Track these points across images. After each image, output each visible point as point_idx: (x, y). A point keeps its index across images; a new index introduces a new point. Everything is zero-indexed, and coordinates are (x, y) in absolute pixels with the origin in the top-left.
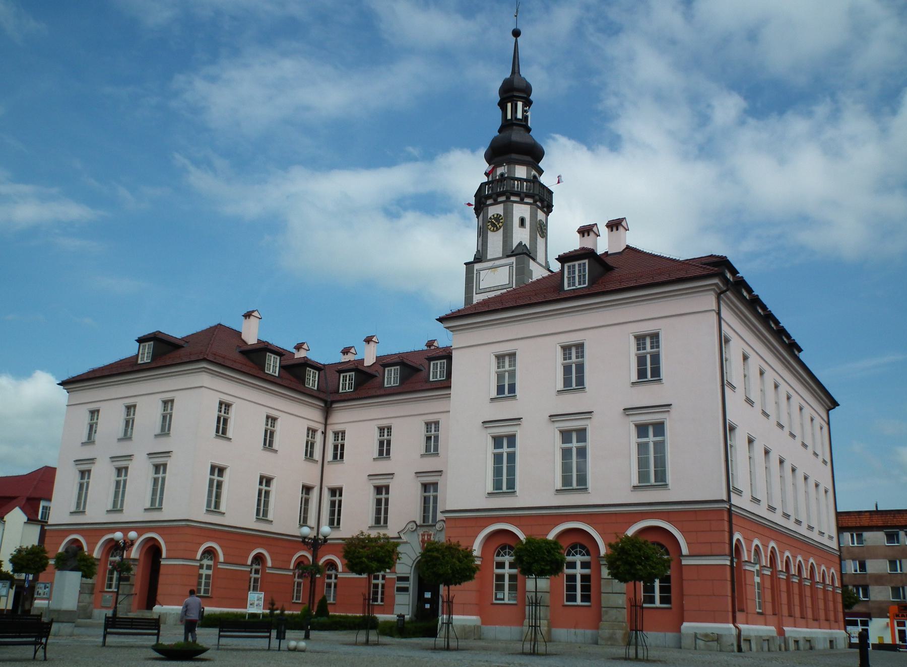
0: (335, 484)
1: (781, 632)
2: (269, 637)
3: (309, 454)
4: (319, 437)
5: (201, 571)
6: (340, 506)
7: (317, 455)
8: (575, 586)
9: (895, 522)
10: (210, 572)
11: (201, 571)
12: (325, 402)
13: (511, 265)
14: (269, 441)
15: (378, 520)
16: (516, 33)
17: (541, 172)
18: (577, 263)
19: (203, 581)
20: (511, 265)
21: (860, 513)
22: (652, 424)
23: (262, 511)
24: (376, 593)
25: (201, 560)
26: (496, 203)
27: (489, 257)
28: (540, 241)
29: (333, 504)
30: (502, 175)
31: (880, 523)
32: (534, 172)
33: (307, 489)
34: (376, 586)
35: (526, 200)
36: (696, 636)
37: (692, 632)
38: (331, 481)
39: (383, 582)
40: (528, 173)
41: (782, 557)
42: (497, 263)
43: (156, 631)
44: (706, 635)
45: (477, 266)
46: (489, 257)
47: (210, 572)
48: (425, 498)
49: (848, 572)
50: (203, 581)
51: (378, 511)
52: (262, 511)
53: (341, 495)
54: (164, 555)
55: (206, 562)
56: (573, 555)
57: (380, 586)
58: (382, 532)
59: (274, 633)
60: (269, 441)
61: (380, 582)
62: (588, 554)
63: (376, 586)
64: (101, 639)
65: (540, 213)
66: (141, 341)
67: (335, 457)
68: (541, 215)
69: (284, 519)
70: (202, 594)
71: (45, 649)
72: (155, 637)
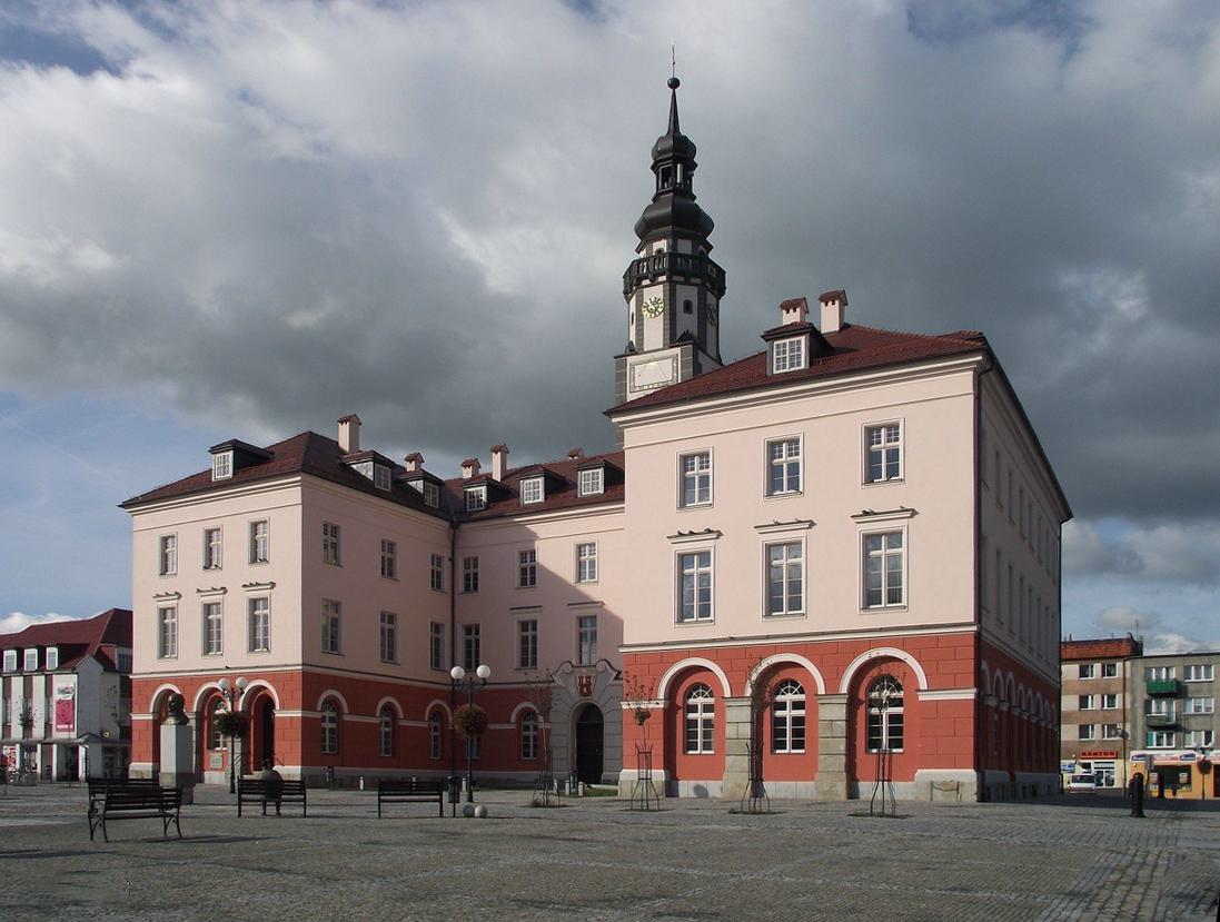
0: (469, 621)
1: (1013, 777)
2: (440, 801)
3: (436, 584)
4: (446, 564)
5: (324, 725)
6: (477, 645)
7: (446, 585)
8: (529, 752)
9: (1091, 653)
10: (333, 726)
11: (324, 725)
12: (452, 522)
13: (675, 358)
14: (388, 569)
15: (524, 662)
16: (674, 84)
17: (710, 247)
18: (787, 341)
19: (789, 738)
20: (675, 358)
21: (1096, 642)
22: (886, 534)
23: (389, 653)
24: (527, 746)
25: (322, 711)
26: (654, 283)
27: (645, 350)
28: (710, 329)
29: (468, 644)
30: (659, 251)
31: (1075, 655)
32: (701, 248)
33: (437, 628)
34: (527, 738)
35: (693, 280)
36: (932, 785)
37: (928, 780)
38: (465, 618)
39: (536, 733)
40: (694, 248)
41: (1017, 689)
42: (656, 355)
43: (438, 797)
44: (945, 783)
45: (630, 359)
46: (645, 350)
47: (333, 726)
48: (581, 634)
49: (299, 772)
50: (789, 738)
51: (524, 651)
52: (389, 653)
53: (477, 633)
54: (277, 707)
55: (328, 714)
56: (783, 694)
57: (531, 739)
58: (532, 675)
59: (446, 795)
60: (388, 569)
61: (531, 733)
62: (801, 691)
63: (527, 738)
64: (237, 808)
65: (709, 295)
66: (215, 450)
67: (467, 588)
68: (711, 298)
69: (412, 664)
70: (327, 751)
71: (177, 822)
72: (438, 804)
